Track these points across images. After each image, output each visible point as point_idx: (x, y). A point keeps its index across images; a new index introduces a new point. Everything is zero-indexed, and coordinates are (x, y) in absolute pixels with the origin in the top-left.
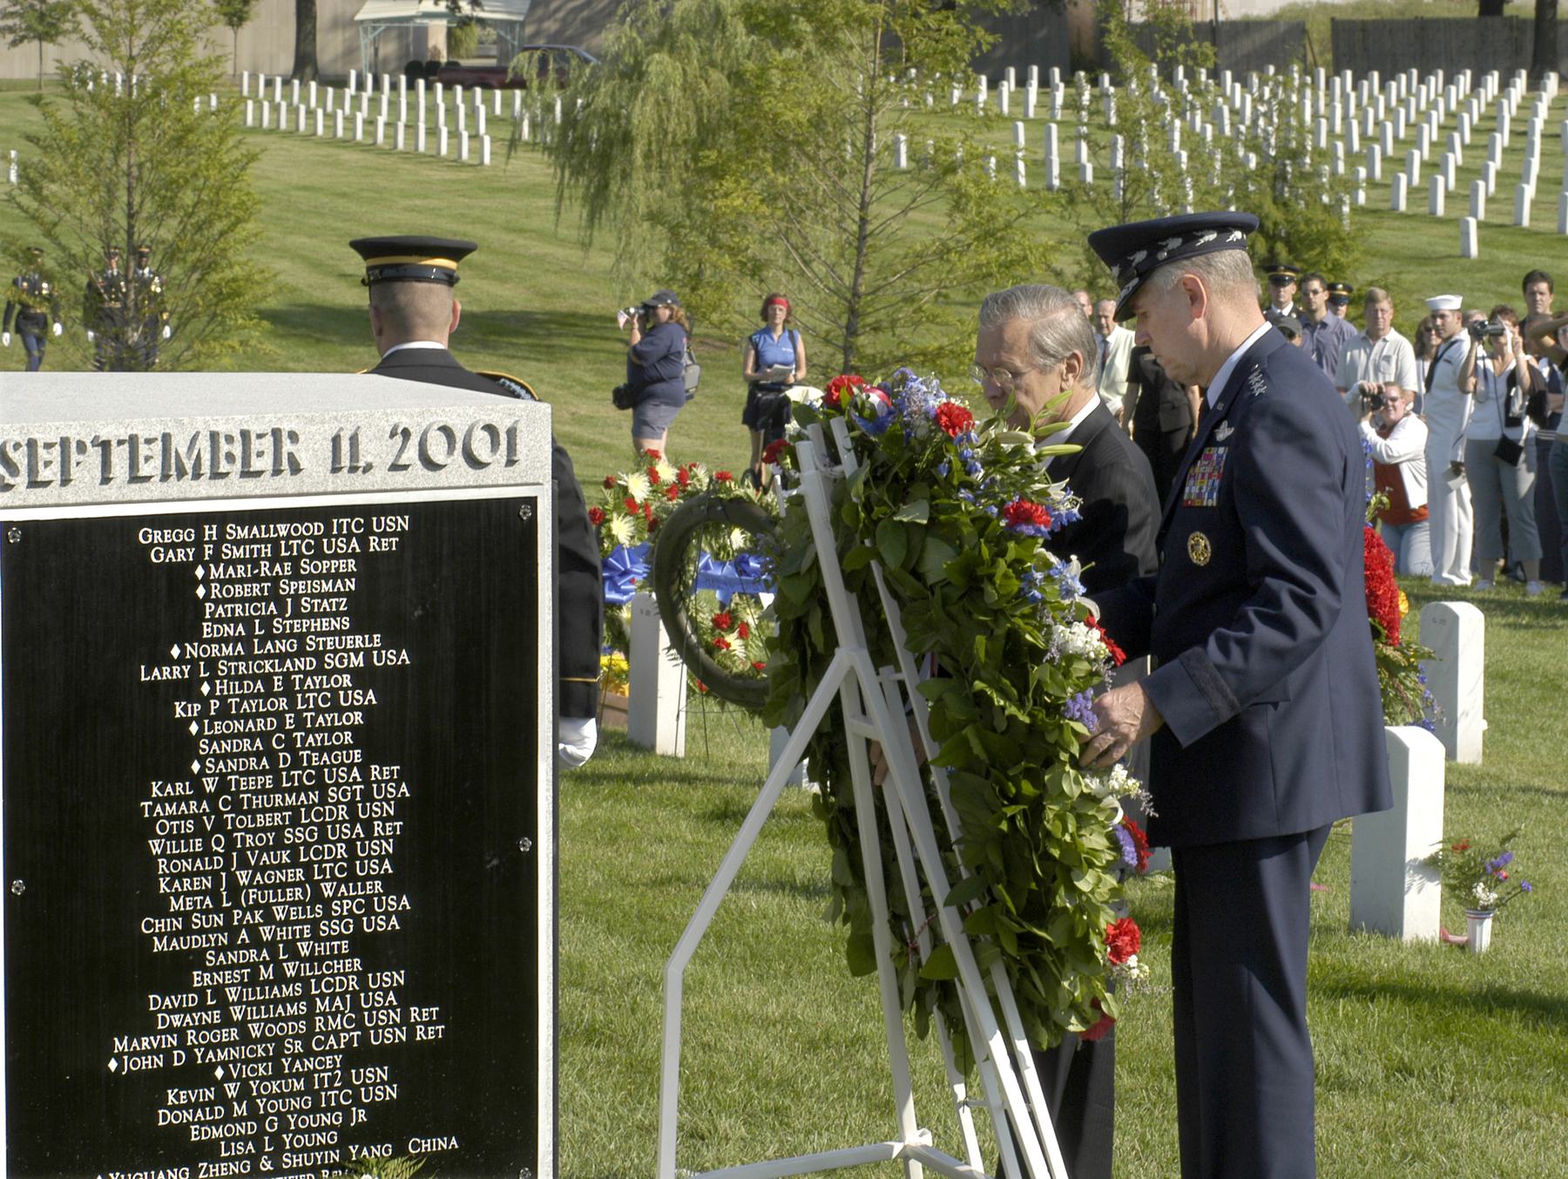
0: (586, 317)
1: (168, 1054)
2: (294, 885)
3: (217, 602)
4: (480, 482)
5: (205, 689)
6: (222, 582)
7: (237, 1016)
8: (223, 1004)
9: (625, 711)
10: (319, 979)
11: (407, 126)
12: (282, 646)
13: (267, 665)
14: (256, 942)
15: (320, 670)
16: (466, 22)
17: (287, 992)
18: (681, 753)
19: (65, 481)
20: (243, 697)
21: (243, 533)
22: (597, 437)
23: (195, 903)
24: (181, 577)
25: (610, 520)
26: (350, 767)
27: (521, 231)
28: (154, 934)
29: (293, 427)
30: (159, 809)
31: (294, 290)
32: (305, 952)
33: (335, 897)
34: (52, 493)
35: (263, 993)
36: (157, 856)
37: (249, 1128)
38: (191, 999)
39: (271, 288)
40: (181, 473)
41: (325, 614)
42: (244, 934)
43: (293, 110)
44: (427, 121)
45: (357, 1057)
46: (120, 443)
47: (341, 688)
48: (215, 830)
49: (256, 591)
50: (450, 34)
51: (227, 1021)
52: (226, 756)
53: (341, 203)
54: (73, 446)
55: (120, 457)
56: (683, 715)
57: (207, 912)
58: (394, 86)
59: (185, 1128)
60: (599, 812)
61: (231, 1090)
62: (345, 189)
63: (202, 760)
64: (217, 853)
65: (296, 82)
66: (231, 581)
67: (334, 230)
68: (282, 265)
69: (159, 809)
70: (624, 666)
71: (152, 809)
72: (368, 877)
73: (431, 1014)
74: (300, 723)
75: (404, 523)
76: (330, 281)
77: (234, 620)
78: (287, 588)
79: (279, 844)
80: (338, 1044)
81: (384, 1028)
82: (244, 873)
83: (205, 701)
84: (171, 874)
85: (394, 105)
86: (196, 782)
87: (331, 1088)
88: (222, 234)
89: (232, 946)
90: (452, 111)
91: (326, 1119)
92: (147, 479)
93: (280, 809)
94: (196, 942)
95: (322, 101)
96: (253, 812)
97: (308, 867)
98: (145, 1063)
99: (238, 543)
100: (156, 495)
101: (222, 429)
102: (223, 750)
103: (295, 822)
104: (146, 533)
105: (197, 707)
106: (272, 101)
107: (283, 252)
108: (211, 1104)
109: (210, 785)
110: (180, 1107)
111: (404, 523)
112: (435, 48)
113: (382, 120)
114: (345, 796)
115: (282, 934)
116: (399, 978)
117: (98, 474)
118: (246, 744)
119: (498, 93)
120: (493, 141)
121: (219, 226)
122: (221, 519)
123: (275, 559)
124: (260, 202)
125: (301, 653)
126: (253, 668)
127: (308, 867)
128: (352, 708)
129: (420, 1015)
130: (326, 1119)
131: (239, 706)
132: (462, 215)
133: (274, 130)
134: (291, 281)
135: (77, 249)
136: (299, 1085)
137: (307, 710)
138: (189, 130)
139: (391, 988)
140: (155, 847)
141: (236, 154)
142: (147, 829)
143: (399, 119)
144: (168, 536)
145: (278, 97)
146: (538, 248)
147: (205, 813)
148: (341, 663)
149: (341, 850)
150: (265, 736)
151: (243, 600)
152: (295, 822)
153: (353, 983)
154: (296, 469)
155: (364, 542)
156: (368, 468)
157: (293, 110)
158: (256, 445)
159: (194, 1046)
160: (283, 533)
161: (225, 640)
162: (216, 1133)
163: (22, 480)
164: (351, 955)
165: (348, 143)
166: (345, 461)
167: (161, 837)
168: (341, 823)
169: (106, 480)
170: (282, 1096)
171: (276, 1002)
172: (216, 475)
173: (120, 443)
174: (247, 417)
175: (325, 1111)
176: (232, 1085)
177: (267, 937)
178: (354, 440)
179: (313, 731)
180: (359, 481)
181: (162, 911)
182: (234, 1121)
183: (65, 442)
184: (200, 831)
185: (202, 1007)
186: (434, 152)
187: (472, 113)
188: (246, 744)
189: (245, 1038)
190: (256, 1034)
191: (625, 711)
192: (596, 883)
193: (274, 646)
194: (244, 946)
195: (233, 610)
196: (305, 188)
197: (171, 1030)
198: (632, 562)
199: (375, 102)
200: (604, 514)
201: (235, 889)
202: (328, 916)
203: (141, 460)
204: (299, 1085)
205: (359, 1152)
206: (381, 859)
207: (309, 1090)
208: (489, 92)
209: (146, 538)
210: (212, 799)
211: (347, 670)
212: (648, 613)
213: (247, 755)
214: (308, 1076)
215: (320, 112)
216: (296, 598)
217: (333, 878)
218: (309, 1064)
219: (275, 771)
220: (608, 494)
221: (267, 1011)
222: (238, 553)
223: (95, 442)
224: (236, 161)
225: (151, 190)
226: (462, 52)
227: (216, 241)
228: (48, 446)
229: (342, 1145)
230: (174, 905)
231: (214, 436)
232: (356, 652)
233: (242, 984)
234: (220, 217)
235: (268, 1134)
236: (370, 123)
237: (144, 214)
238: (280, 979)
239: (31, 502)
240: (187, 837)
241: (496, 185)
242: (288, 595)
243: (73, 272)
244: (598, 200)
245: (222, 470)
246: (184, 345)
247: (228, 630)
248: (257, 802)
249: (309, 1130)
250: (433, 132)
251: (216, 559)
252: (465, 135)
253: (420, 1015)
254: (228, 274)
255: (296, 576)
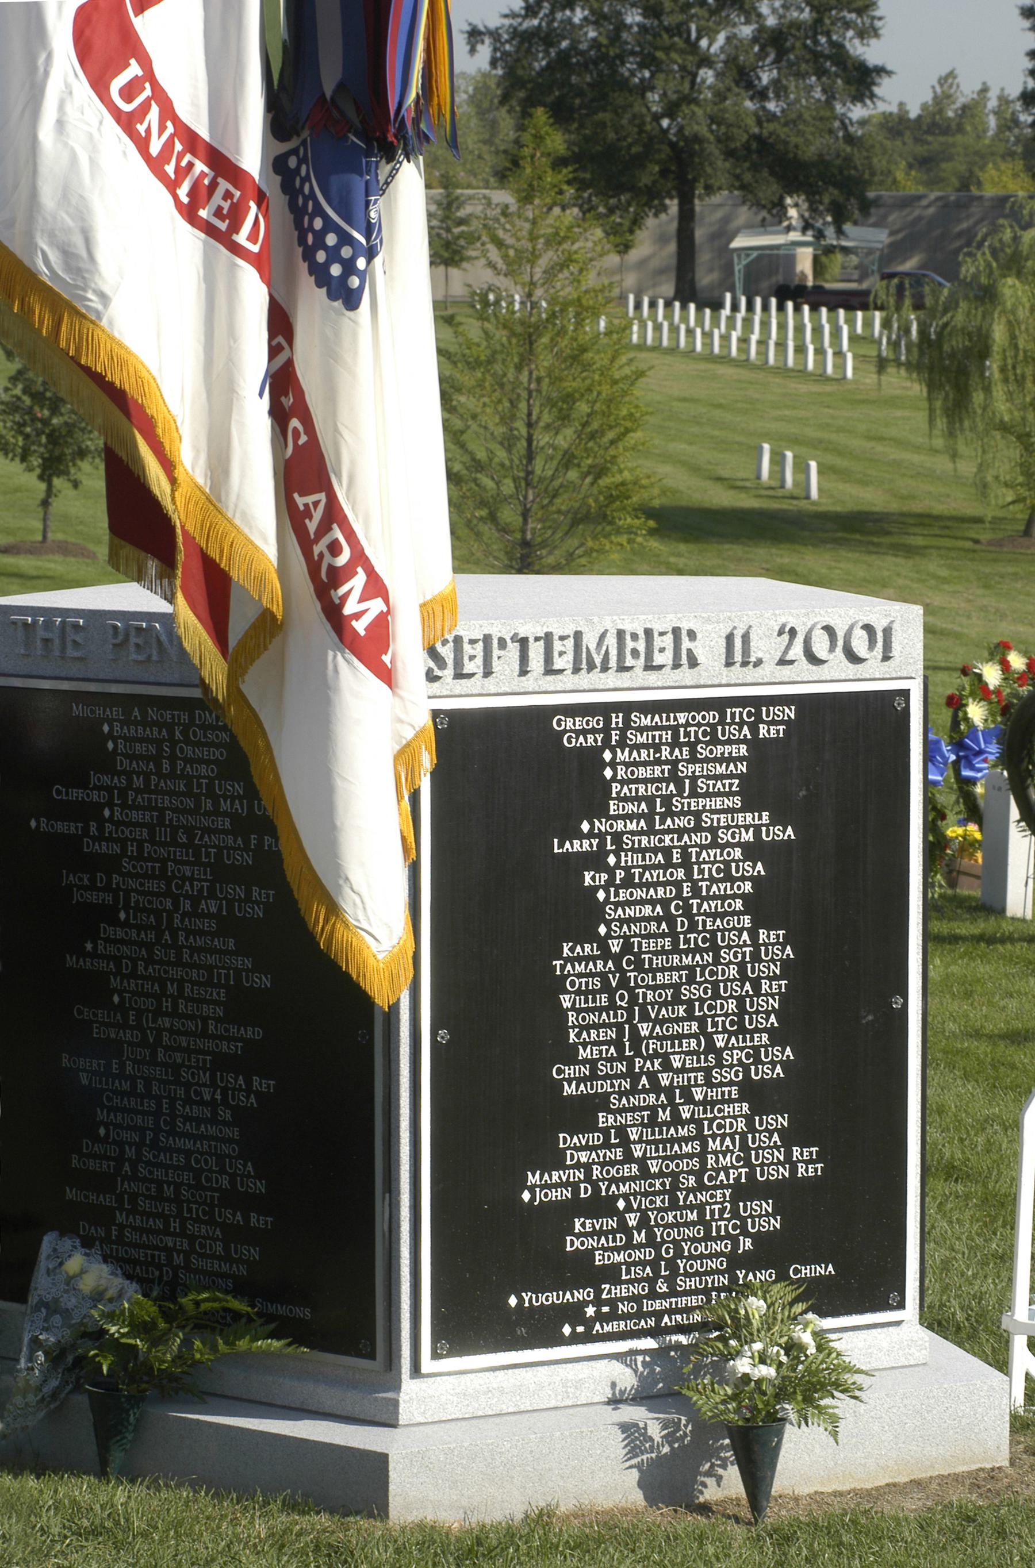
0: (938, 518)
1: (575, 1187)
2: (689, 1036)
3: (622, 782)
4: (859, 676)
5: (612, 860)
6: (627, 765)
7: (638, 1154)
8: (625, 1142)
9: (977, 877)
10: (711, 1121)
11: (777, 344)
12: (682, 822)
13: (667, 838)
14: (656, 1087)
15: (714, 844)
16: (829, 250)
17: (683, 1132)
18: (1029, 916)
19: (488, 673)
20: (645, 868)
21: (646, 721)
22: (950, 626)
23: (601, 1052)
24: (590, 760)
25: (966, 705)
26: (740, 931)
27: (881, 439)
28: (564, 1079)
29: (693, 627)
30: (569, 967)
31: (675, 492)
32: (699, 1097)
33: (726, 1048)
34: (476, 684)
35: (661, 1133)
36: (568, 1009)
37: (649, 1253)
38: (595, 1138)
39: (656, 491)
40: (591, 667)
41: (719, 794)
42: (644, 1080)
43: (674, 330)
44: (795, 339)
45: (745, 1191)
46: (537, 639)
47: (733, 860)
48: (620, 986)
49: (657, 772)
50: (816, 260)
51: (628, 1158)
52: (629, 921)
53: (717, 413)
54: (495, 642)
55: (536, 652)
56: (1031, 882)
57: (611, 1060)
58: (766, 308)
59: (590, 1253)
60: (954, 969)
61: (632, 1220)
62: (722, 401)
63: (608, 924)
64: (621, 1007)
65: (677, 304)
66: (636, 764)
67: (712, 437)
68: (664, 469)
69: (569, 967)
70: (978, 836)
71: (563, 967)
72: (757, 1030)
73: (811, 1153)
74: (696, 892)
75: (791, 713)
76: (709, 484)
77: (638, 799)
78: (686, 770)
79: (677, 1000)
80: (728, 1179)
81: (769, 1165)
82: (645, 1025)
83: (611, 872)
84: (580, 1026)
85: (765, 325)
86: (603, 944)
87: (721, 1219)
88: (612, 442)
89: (634, 1091)
90: (817, 330)
91: (716, 1247)
92: (560, 671)
93: (678, 969)
94: (602, 1087)
95: (700, 321)
96: (654, 971)
97: (702, 1021)
98: (554, 1195)
99: (641, 730)
100: (569, 686)
101: (628, 627)
102: (628, 913)
103: (691, 980)
104: (560, 720)
105: (604, 877)
106: (655, 321)
107: (666, 458)
108: (613, 1232)
109: (615, 946)
110: (586, 1235)
111: (791, 713)
112: (802, 273)
113: (754, 338)
114: (736, 957)
115: (678, 1080)
116: (783, 1121)
117: (517, 667)
118: (647, 911)
119: (860, 314)
120: (855, 357)
121: (611, 435)
122: (627, 708)
123: (675, 744)
124: (647, 413)
125: (698, 828)
126: (654, 841)
127: (702, 1021)
128: (743, 879)
129: (802, 1154)
130: (716, 1247)
131: (641, 875)
132: (828, 425)
133: (657, 348)
134: (669, 483)
135: (481, 455)
136: (693, 1216)
137: (703, 880)
138: (583, 350)
139: (776, 1129)
140: (566, 1001)
141: (627, 371)
142: (559, 985)
143: (769, 337)
144: (580, 723)
145: (660, 318)
146: (895, 454)
147: (610, 971)
148: (733, 838)
149: (732, 1006)
150: (665, 903)
151: (645, 781)
152: (691, 980)
153: (741, 1125)
154: (693, 663)
155: (754, 729)
156: (759, 663)
157: (674, 330)
158: (658, 642)
159: (599, 1180)
160: (682, 721)
161: (630, 817)
162: (618, 1258)
163: (449, 672)
164: (739, 1100)
165: (724, 359)
166: (738, 657)
167: (570, 993)
168: (732, 981)
169: (524, 672)
170: (677, 1225)
171: (672, 1141)
172: (622, 668)
173: (537, 639)
174: (650, 617)
175: (714, 1240)
176: (632, 1215)
177: (665, 1082)
178: (746, 638)
179: (708, 898)
180: (750, 674)
181: (572, 1059)
182: (634, 1247)
183: (487, 639)
184: (606, 987)
185: (607, 1145)
186: (801, 368)
187: (836, 333)
188: (647, 911)
189: (645, 1173)
190: (654, 1169)
191: (977, 877)
192: (953, 1033)
193: (673, 822)
194: (645, 1091)
195: (637, 789)
196: (685, 400)
197: (578, 1165)
198: (985, 742)
199: (748, 322)
200: (961, 697)
201: (636, 1040)
202: (720, 1065)
203: (556, 654)
204: (693, 1216)
205: (746, 1276)
206: (768, 1014)
207: (701, 1220)
208: (851, 313)
209: (559, 725)
210: (617, 959)
211: (739, 844)
212: (1000, 789)
213: (648, 919)
214: (701, 1208)
215: (698, 331)
216: (694, 779)
217: (725, 1030)
218: (702, 1197)
219: (673, 934)
220: (966, 681)
221: (665, 1150)
222: (642, 739)
223: (513, 639)
224: (626, 377)
225: (550, 402)
226: (828, 277)
227: (607, 449)
228: (472, 642)
229: (731, 1271)
230: (583, 1054)
231: (620, 634)
232: (747, 828)
233: (643, 1125)
234: (611, 427)
235: (664, 1259)
236: (744, 341)
237: (541, 424)
238: (677, 1120)
239: (457, 692)
240: (594, 992)
241: (859, 397)
242: (687, 777)
243: (479, 475)
244: (957, 409)
245: (627, 664)
246: (576, 542)
247: (631, 808)
248: (658, 961)
249: (701, 1256)
250: (801, 349)
251: (622, 744)
252: (830, 352)
253: (802, 1154)
254: (618, 479)
255: (693, 759)
